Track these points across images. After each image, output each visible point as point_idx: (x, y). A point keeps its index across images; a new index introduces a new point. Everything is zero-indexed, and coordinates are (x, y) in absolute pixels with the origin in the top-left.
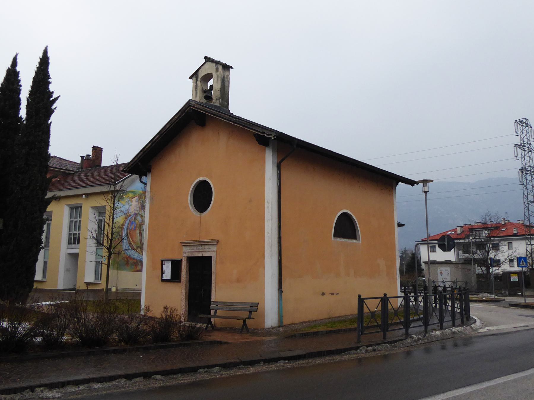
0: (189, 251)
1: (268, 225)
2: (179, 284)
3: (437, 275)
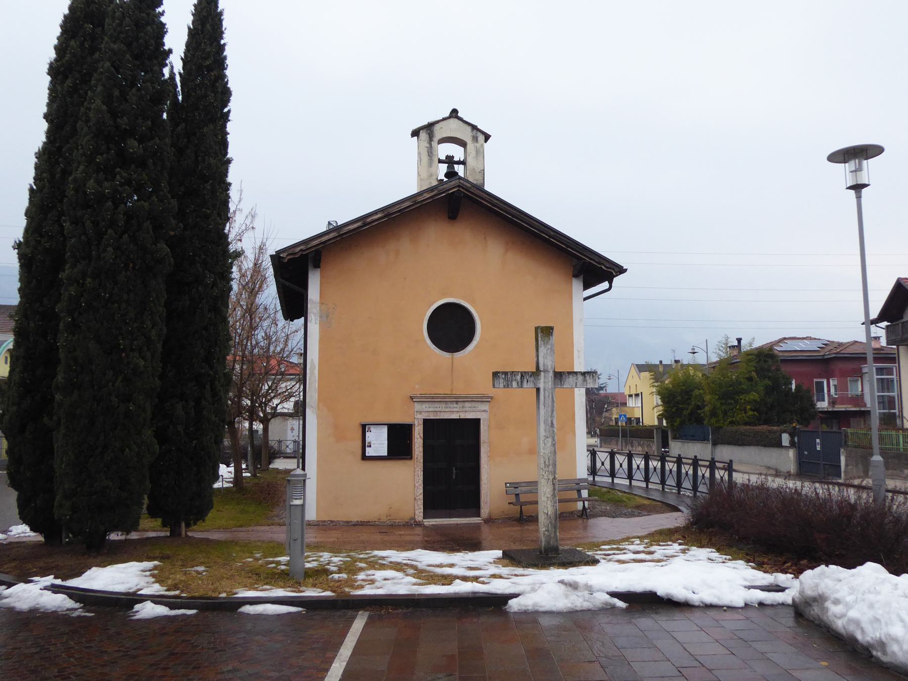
3: (286, 430)
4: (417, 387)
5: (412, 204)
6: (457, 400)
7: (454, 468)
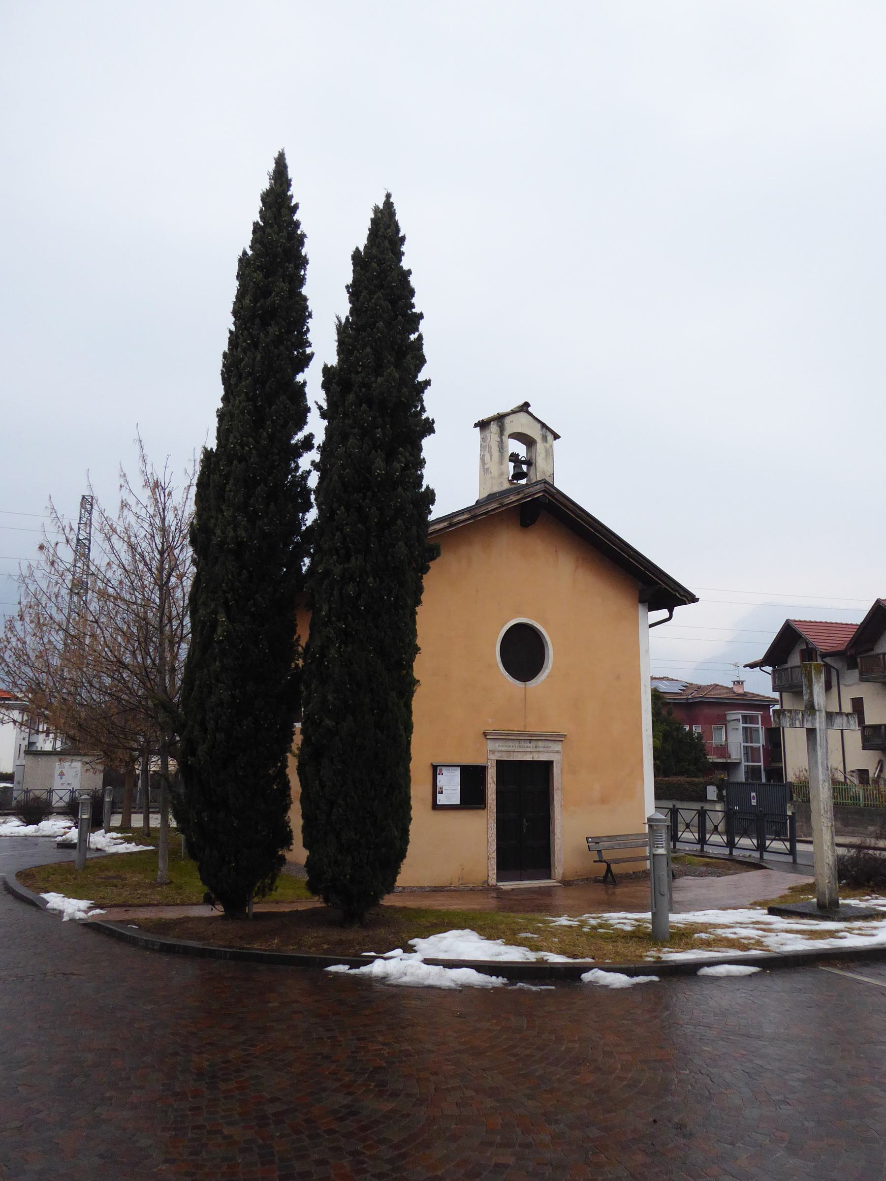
0: (504, 749)
1: (647, 719)
2: (482, 812)
3: (52, 776)
4: (490, 721)
5: (498, 506)
6: (532, 738)
7: (525, 820)
